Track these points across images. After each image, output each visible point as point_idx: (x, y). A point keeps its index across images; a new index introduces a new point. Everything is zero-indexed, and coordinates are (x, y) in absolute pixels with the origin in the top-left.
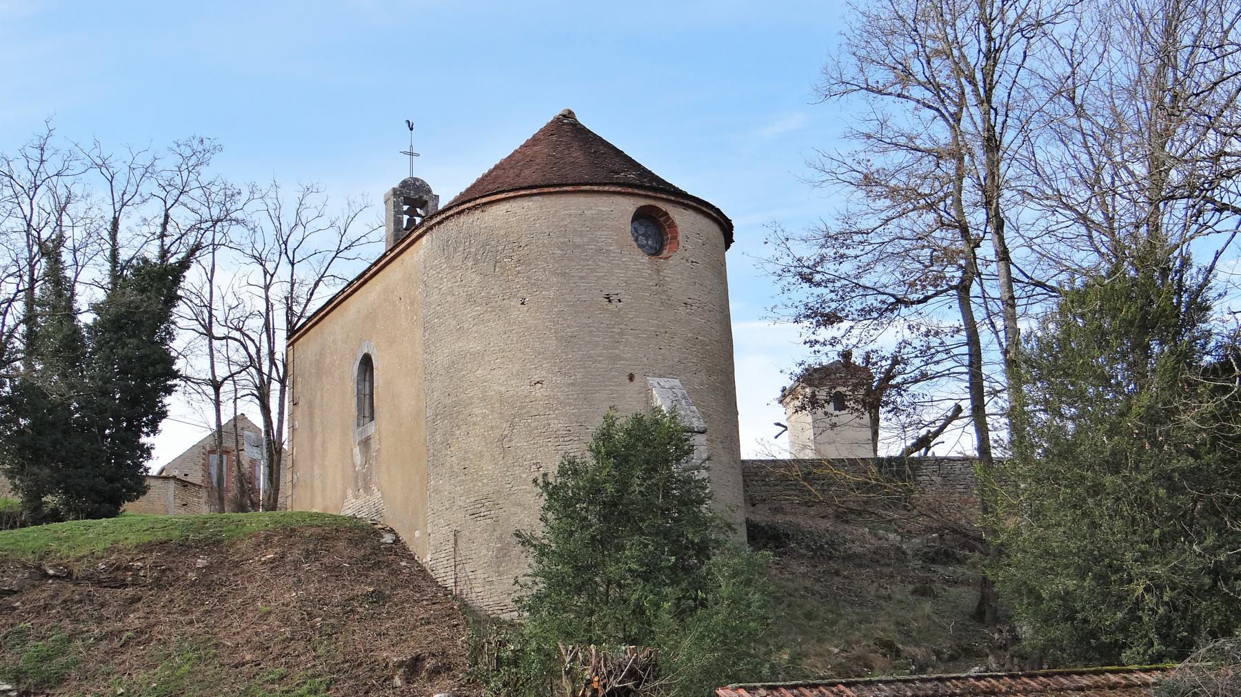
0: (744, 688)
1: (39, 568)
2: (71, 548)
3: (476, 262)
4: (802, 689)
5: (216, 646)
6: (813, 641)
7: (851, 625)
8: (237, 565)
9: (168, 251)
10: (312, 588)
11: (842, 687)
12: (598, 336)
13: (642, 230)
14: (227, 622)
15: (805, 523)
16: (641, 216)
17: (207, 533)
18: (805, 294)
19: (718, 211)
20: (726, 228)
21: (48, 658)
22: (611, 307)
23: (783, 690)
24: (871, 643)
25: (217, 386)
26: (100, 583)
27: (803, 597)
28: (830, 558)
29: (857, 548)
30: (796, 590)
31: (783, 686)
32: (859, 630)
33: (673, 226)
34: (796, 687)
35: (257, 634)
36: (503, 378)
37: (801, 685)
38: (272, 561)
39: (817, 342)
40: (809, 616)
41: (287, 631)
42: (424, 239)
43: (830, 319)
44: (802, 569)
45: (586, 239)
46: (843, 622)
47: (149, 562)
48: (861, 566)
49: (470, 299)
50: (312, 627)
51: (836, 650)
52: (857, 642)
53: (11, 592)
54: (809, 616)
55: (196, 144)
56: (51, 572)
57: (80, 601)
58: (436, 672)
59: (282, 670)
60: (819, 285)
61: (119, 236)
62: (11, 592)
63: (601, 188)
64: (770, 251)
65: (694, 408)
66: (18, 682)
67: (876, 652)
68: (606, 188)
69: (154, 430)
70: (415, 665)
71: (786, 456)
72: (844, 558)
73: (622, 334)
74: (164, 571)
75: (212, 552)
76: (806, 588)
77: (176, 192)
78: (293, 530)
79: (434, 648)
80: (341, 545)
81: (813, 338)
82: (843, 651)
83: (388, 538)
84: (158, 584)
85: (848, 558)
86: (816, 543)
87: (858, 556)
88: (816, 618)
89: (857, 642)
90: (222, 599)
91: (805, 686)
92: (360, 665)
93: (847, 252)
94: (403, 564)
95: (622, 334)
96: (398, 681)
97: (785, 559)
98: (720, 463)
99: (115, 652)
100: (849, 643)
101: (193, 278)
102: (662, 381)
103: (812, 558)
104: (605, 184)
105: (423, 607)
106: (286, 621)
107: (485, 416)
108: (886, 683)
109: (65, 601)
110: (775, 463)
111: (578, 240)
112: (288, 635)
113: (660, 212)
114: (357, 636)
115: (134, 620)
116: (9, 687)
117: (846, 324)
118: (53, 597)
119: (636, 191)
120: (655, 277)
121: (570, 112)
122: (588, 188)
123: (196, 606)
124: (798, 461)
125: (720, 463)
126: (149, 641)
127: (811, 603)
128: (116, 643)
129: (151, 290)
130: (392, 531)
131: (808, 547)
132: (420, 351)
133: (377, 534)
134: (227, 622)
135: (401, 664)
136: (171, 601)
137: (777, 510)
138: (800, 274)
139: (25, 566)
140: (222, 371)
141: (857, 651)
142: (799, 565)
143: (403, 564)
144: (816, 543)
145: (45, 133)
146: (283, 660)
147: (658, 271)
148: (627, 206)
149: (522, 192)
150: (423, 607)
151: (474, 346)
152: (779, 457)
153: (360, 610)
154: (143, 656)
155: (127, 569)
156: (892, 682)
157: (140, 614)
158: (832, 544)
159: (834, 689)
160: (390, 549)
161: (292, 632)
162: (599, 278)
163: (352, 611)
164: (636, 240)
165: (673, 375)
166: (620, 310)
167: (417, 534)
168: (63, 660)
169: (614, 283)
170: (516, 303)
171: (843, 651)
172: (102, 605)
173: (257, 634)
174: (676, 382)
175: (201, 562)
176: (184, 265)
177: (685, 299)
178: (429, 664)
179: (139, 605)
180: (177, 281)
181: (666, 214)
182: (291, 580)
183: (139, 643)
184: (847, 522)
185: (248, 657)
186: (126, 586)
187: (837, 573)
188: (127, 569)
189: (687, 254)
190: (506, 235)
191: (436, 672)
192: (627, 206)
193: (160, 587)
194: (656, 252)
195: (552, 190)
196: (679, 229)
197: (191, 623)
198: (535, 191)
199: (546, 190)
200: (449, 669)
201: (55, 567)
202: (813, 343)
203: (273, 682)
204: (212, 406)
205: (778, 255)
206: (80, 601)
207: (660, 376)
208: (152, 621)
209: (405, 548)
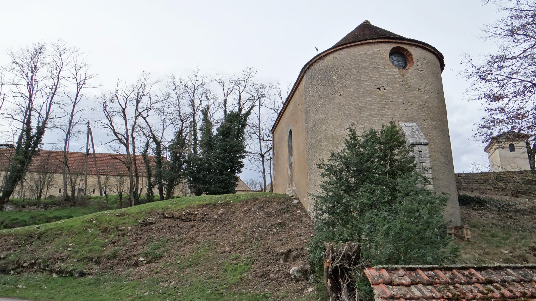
0: (387, 269)
1: (163, 214)
2: (175, 207)
3: (322, 81)
4: (437, 271)
5: (217, 244)
6: (493, 247)
7: (516, 240)
8: (233, 212)
9: (242, 108)
10: (258, 221)
11: (473, 271)
12: (375, 106)
13: (395, 58)
14: (224, 235)
15: (495, 197)
16: (393, 52)
17: (225, 201)
18: (485, 87)
19: (434, 48)
20: (440, 57)
21: (158, 248)
22: (381, 92)
23: (420, 271)
24: (527, 249)
25: (262, 156)
26: (182, 220)
27: (491, 227)
28: (507, 211)
29: (522, 207)
30: (488, 224)
31: (420, 268)
32: (520, 242)
33: (410, 55)
34: (432, 269)
35: (232, 240)
36: (333, 128)
37: (437, 268)
38: (246, 211)
39: (491, 109)
40: (493, 236)
41: (243, 239)
42: (304, 78)
43: (497, 98)
44: (493, 215)
45: (367, 64)
46: (513, 238)
47: (201, 212)
48: (523, 214)
49: (320, 97)
50: (253, 237)
51: (506, 252)
52: (519, 248)
53: (152, 223)
54: (493, 236)
55: (248, 70)
56: (167, 216)
57: (174, 227)
58: (297, 257)
59: (238, 254)
60: (489, 81)
61: (227, 105)
62: (152, 223)
63: (374, 41)
64: (463, 67)
65: (422, 134)
66: (147, 257)
67: (530, 253)
68: (376, 40)
69: (240, 172)
70: (289, 254)
71: (486, 170)
72: (514, 211)
73: (386, 104)
74: (205, 215)
75: (226, 208)
76: (493, 224)
77: (243, 88)
78: (257, 199)
79: (298, 247)
80: (274, 204)
81: (489, 107)
82: (509, 252)
83: (295, 202)
84: (202, 220)
85: (517, 211)
86: (500, 205)
87: (523, 210)
88: (497, 237)
89: (519, 248)
90: (224, 226)
91: (440, 269)
92: (268, 253)
93: (504, 64)
94: (298, 212)
95: (386, 104)
96: (281, 261)
97: (484, 211)
98: (440, 162)
99: (182, 246)
100: (514, 249)
101: (252, 119)
102: (407, 124)
103: (498, 211)
104: (376, 39)
105: (301, 229)
106: (244, 234)
107: (326, 146)
108: (514, 268)
109: (169, 227)
110: (482, 174)
111: (364, 65)
112: (243, 240)
113: (402, 50)
114: (270, 240)
115: (191, 234)
116: (143, 259)
117: (506, 100)
118: (165, 225)
119: (391, 40)
120: (402, 77)
121: (367, 21)
122: (368, 41)
123: (214, 229)
124: (494, 173)
125: (440, 162)
126: (194, 242)
127: (495, 230)
128: (183, 243)
129: (236, 122)
130: (298, 199)
131: (496, 206)
132: (304, 123)
133: (291, 199)
134: (224, 235)
135: (282, 254)
136: (206, 227)
137: (482, 193)
138: (479, 76)
139: (158, 214)
140: (264, 150)
141: (518, 253)
142: (491, 214)
143: (298, 212)
144: (500, 205)
145: (196, 71)
146: (239, 251)
147: (403, 75)
148: (388, 48)
149: (339, 48)
150: (301, 229)
151: (322, 116)
152: (484, 171)
153: (274, 230)
154: (190, 248)
155: (192, 214)
156: (520, 268)
157: (194, 232)
158: (508, 205)
159: (466, 273)
160: (295, 206)
161: (245, 239)
162: (374, 80)
163: (271, 230)
164: (393, 63)
165: (412, 121)
166: (385, 93)
167: (305, 199)
168: (163, 249)
169: (381, 82)
170: (337, 95)
171: (509, 252)
172: (181, 228)
173: (232, 240)
174: (414, 124)
175: (220, 212)
176: (248, 113)
177: (418, 87)
178: (294, 253)
179: (194, 228)
180: (245, 120)
181: (407, 50)
182: (251, 218)
183: (190, 243)
184: (517, 197)
185: (227, 249)
186: (191, 221)
187: (511, 217)
188: (192, 214)
189: (418, 67)
190: (333, 68)
191: (297, 257)
192: (388, 48)
193: (204, 221)
194: (404, 67)
195: (351, 44)
196: (414, 56)
197: (210, 235)
198: (344, 46)
199: (349, 45)
200: (303, 256)
201: (168, 214)
202: (489, 110)
203: (233, 260)
204: (262, 164)
205: (467, 67)
206: (174, 227)
207: (406, 122)
208: (197, 234)
209: (302, 206)
